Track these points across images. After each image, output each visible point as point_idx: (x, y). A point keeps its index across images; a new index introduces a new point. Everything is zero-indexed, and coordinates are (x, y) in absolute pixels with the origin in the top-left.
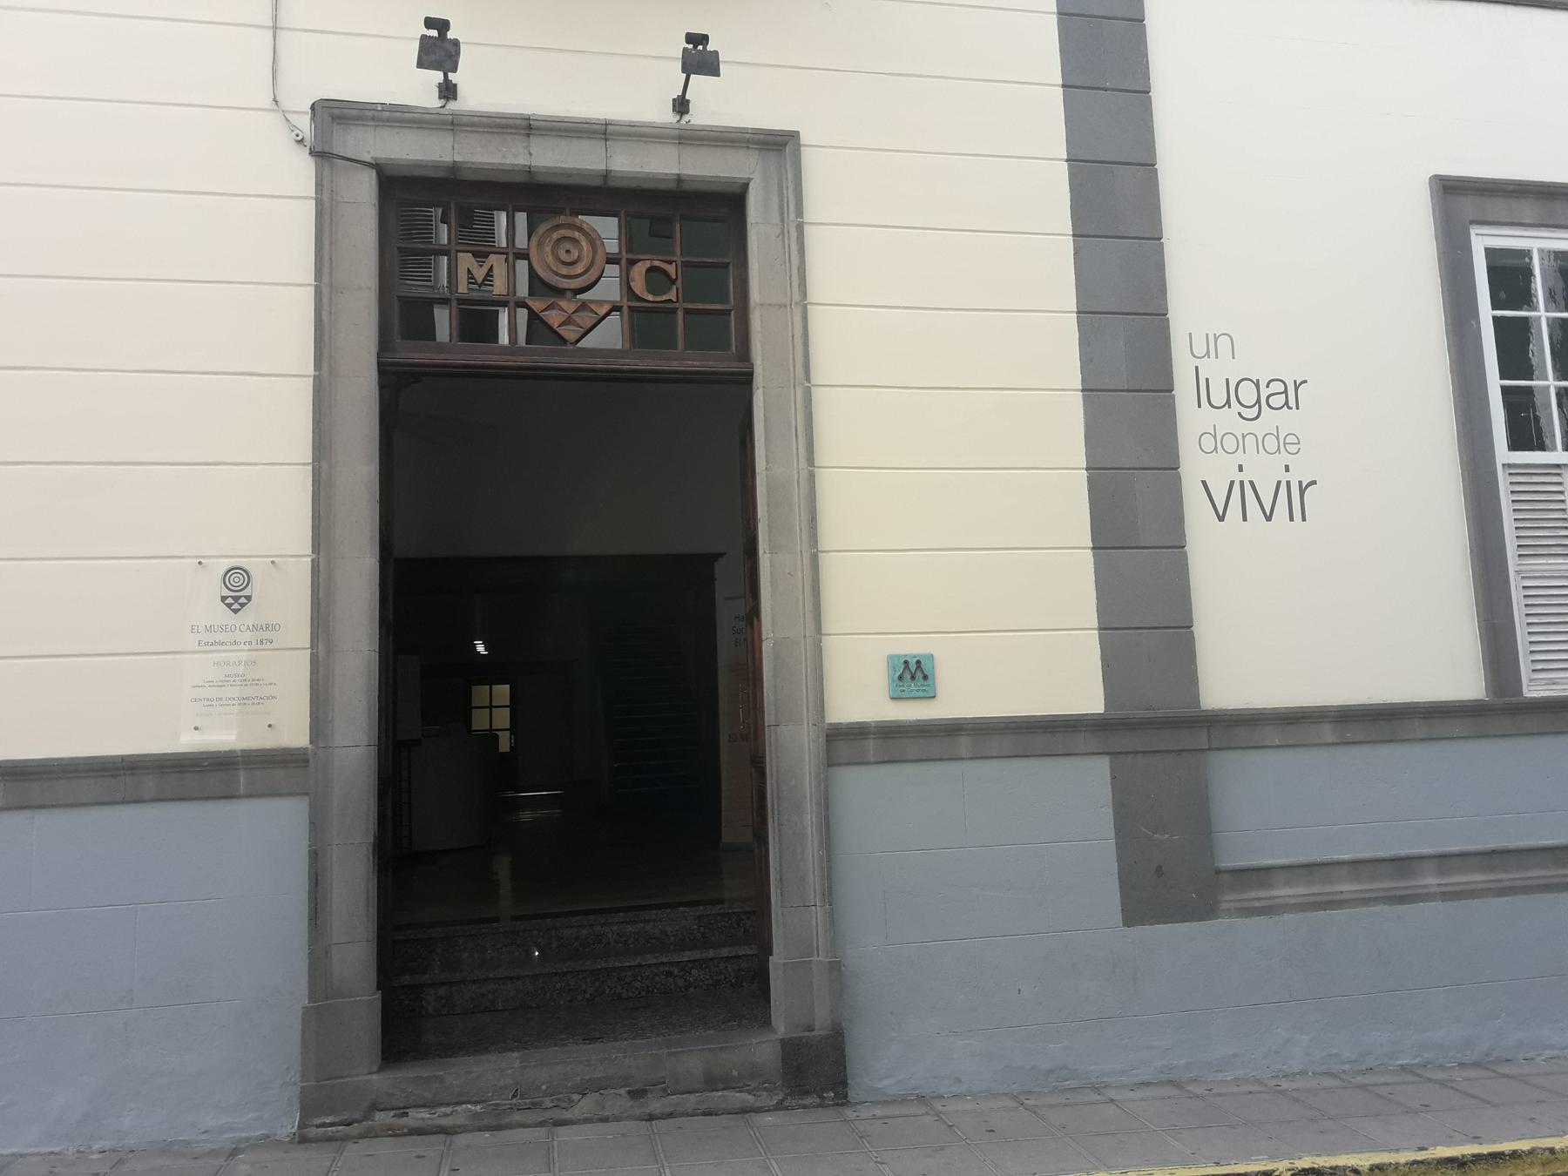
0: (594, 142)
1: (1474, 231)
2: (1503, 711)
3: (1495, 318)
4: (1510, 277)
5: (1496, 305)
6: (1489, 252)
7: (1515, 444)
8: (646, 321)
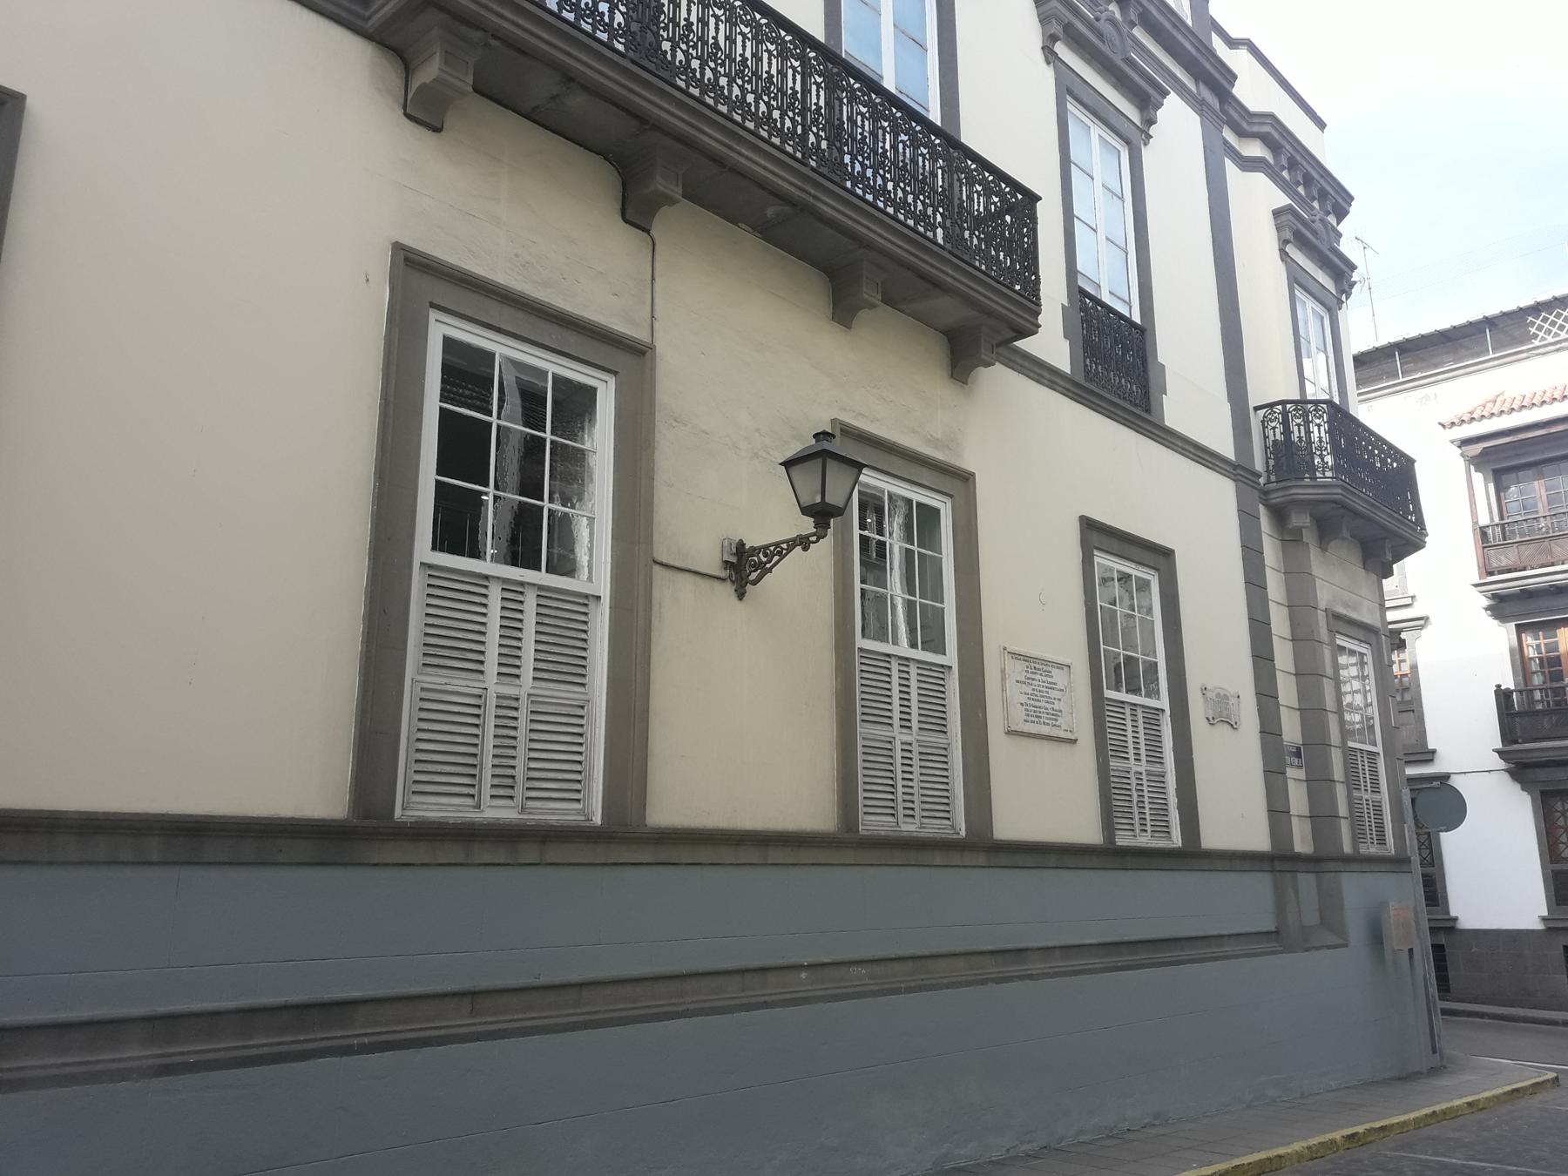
0: (1260, 875)
1: (434, 315)
2: (360, 835)
3: (441, 409)
4: (467, 375)
5: (443, 398)
6: (449, 343)
7: (438, 545)
8: (1350, 705)
